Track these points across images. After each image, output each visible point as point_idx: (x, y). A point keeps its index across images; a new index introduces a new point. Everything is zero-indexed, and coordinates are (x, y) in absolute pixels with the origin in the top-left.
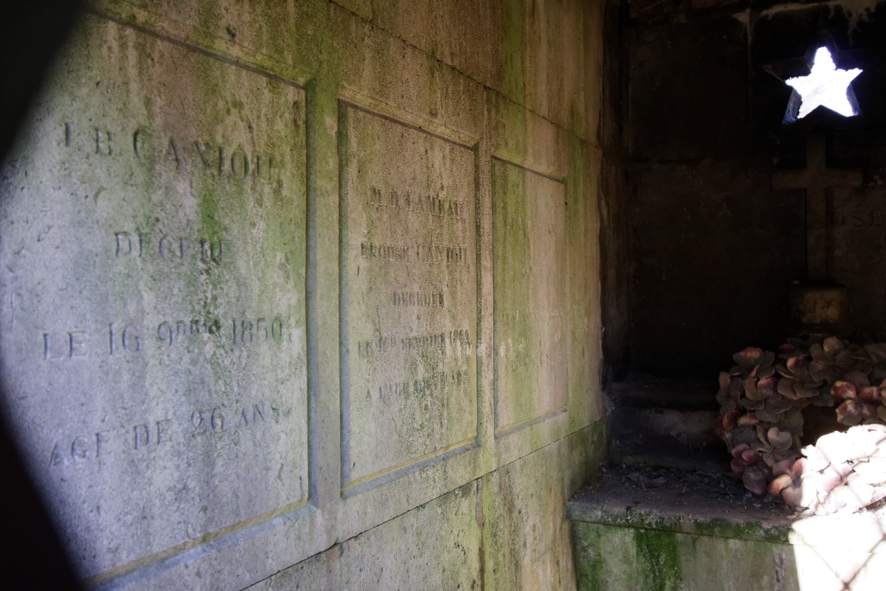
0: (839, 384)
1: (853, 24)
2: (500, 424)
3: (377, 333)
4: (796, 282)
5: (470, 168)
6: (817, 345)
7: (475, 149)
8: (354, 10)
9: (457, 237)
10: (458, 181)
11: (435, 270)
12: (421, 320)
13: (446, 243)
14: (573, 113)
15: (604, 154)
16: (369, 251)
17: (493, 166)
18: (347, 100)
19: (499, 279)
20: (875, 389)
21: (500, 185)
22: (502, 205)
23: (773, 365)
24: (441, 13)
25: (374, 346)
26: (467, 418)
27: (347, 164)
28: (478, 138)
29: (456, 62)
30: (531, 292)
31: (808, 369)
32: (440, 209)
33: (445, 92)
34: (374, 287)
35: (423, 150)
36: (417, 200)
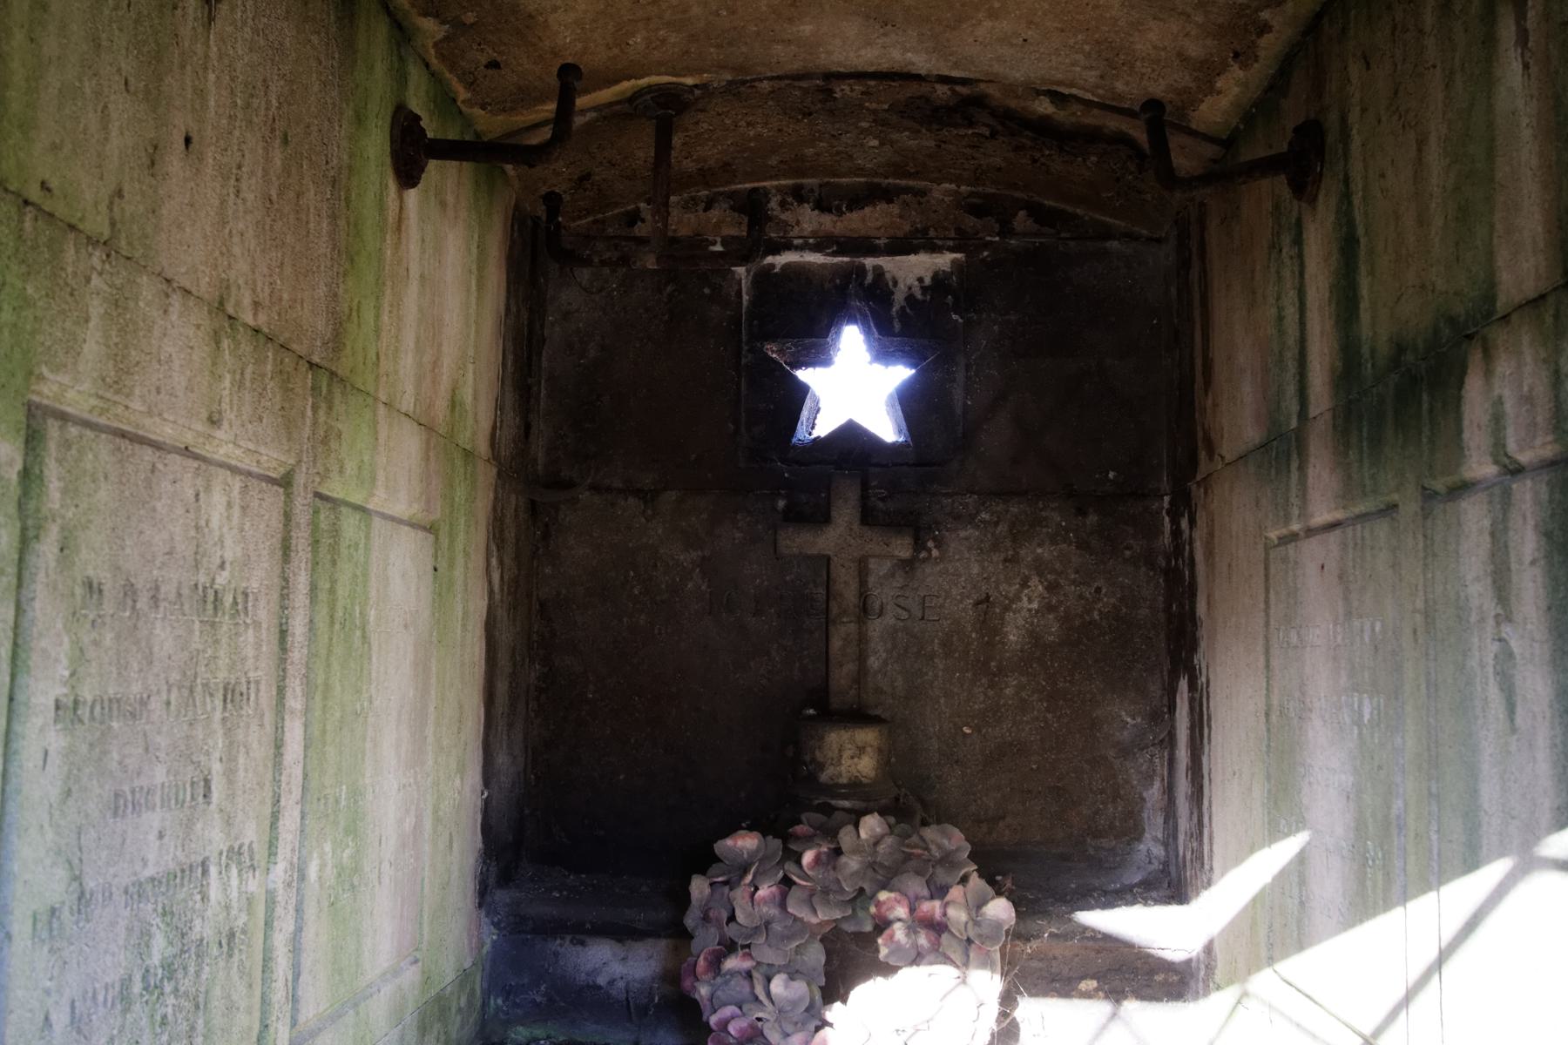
0: (883, 896)
1: (899, 297)
2: (302, 1019)
3: (75, 885)
4: (811, 711)
5: (276, 522)
6: (850, 828)
7: (285, 482)
8: (73, 221)
9: (244, 660)
10: (252, 547)
11: (199, 733)
12: (166, 839)
13: (222, 675)
14: (454, 404)
15: (499, 474)
16: (70, 714)
17: (316, 512)
18: (45, 402)
19: (316, 731)
20: (937, 904)
21: (326, 546)
22: (328, 586)
23: (781, 863)
24: (241, 226)
25: (66, 913)
26: (242, 1020)
27: (37, 537)
28: (292, 461)
29: (262, 319)
30: (368, 745)
31: (834, 868)
32: (215, 608)
33: (238, 377)
34: (75, 788)
35: (190, 493)
36: (172, 596)
